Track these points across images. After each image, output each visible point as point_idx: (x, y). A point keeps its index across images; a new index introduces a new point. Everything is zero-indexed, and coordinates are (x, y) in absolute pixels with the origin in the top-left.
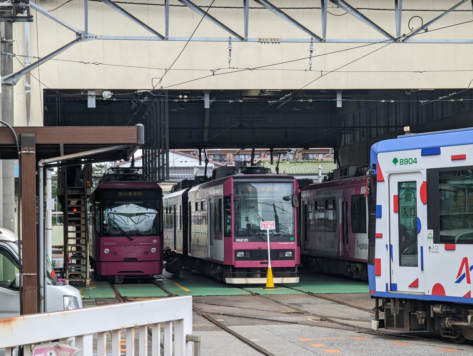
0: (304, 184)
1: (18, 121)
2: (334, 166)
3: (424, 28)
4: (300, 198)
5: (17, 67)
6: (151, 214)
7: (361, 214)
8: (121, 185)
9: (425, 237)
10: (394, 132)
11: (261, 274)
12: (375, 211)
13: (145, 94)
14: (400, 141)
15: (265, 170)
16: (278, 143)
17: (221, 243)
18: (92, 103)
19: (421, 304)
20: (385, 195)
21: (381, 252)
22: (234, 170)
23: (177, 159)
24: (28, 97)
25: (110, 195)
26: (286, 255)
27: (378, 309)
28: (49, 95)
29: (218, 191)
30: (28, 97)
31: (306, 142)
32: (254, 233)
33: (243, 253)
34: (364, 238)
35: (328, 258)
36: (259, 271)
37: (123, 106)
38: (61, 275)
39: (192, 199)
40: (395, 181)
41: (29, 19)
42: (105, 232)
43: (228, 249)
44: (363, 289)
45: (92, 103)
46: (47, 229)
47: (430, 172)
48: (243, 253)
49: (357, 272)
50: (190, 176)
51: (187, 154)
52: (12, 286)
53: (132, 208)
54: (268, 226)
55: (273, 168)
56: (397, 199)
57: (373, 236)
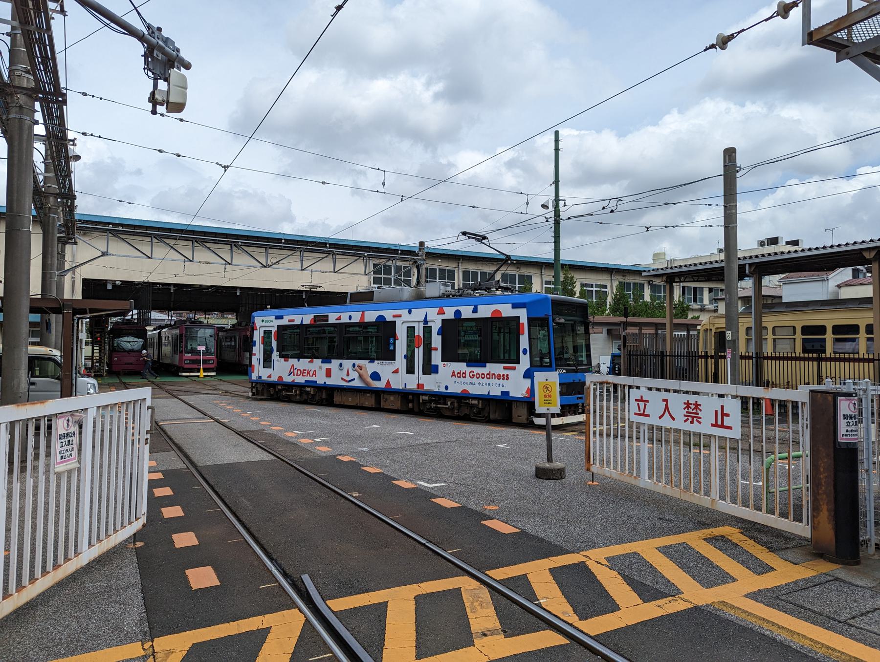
0: (221, 329)
1: (67, 295)
2: (236, 321)
3: (278, 262)
4: (218, 335)
5: (67, 267)
6: (141, 341)
7: (248, 343)
8: (125, 327)
9: (275, 355)
10: (263, 308)
12: (254, 343)
13: (139, 283)
14: (265, 312)
15: (202, 322)
16: (208, 310)
17: (177, 357)
18: (109, 287)
19: (270, 385)
20: (258, 336)
21: (255, 362)
22: (185, 322)
23: (155, 315)
24: (73, 282)
25: (118, 331)
27: (252, 387)
28: (86, 282)
29: (177, 331)
30: (73, 282)
31: (223, 310)
32: (195, 352)
34: (247, 354)
35: (231, 362)
37: (128, 290)
38: (91, 372)
39: (163, 335)
40: (262, 330)
41: (75, 243)
42: (114, 350)
43: (181, 359)
44: (246, 378)
45: (109, 287)
46: (267, 253)
47: (278, 326)
49: (244, 369)
50: (163, 324)
51: (161, 312)
52: (58, 378)
53: (130, 339)
54: (202, 348)
55: (205, 322)
56: (263, 338)
57: (251, 355)
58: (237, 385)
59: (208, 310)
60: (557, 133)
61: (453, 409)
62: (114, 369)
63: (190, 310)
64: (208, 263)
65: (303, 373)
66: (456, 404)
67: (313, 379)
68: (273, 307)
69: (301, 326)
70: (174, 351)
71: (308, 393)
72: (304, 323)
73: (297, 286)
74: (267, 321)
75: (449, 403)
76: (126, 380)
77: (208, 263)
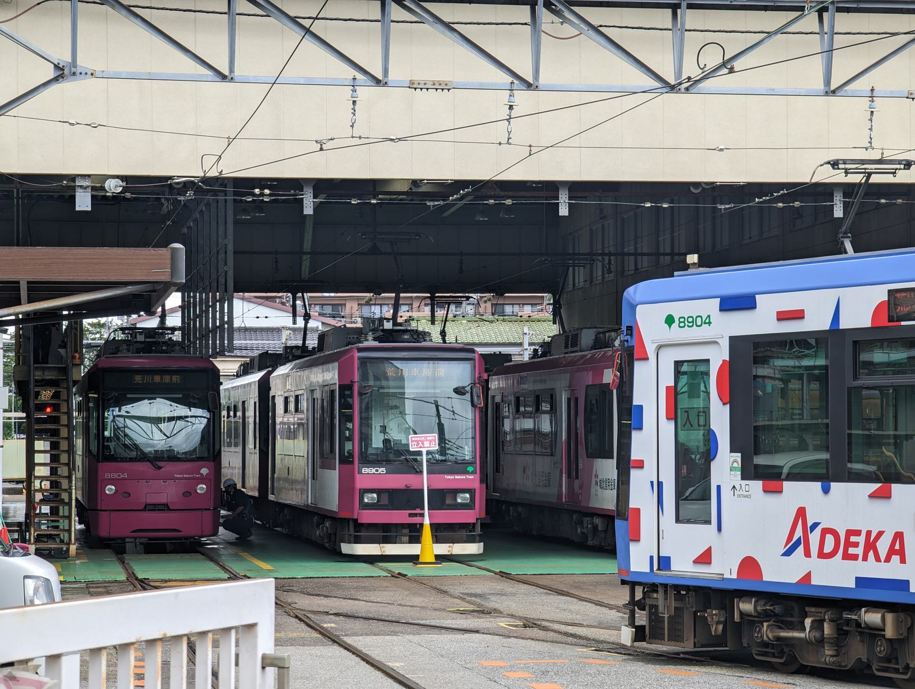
0: (495, 363)
2: (553, 330)
3: (727, 65)
4: (486, 389)
6: (198, 419)
7: (604, 422)
8: (139, 361)
9: (725, 467)
10: (667, 265)
11: (410, 536)
12: (631, 416)
13: (188, 185)
14: (679, 280)
15: (419, 336)
16: (445, 284)
17: (333, 477)
18: (83, 202)
20: (650, 385)
21: (640, 496)
22: (359, 334)
23: (248, 312)
25: (116, 381)
26: (459, 501)
29: (328, 375)
32: (398, 457)
33: (375, 495)
34: (608, 468)
36: (406, 531)
39: (277, 391)
42: (107, 452)
43: (346, 486)
44: (606, 567)
45: (83, 202)
46: (679, 30)
47: (736, 342)
48: (375, 495)
49: (597, 533)
50: (275, 345)
53: (161, 407)
54: (425, 444)
56: (673, 394)
57: (625, 465)
58: (576, 596)
59: (443, 287)
60: (591, 230)
61: (821, 641)
62: (104, 531)
63: (374, 286)
64: (443, 87)
65: (845, 544)
66: (827, 629)
67: (892, 570)
68: (709, 261)
69: (834, 338)
70: (322, 456)
71: (873, 633)
72: (844, 324)
73: (805, 167)
74: (690, 322)
75: (808, 622)
76: (143, 571)
77: (443, 87)
